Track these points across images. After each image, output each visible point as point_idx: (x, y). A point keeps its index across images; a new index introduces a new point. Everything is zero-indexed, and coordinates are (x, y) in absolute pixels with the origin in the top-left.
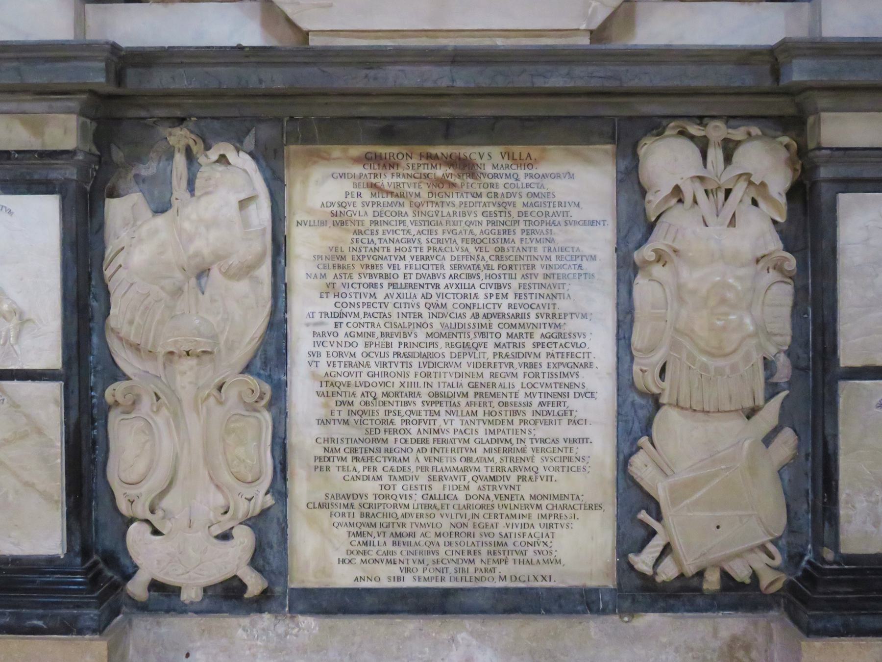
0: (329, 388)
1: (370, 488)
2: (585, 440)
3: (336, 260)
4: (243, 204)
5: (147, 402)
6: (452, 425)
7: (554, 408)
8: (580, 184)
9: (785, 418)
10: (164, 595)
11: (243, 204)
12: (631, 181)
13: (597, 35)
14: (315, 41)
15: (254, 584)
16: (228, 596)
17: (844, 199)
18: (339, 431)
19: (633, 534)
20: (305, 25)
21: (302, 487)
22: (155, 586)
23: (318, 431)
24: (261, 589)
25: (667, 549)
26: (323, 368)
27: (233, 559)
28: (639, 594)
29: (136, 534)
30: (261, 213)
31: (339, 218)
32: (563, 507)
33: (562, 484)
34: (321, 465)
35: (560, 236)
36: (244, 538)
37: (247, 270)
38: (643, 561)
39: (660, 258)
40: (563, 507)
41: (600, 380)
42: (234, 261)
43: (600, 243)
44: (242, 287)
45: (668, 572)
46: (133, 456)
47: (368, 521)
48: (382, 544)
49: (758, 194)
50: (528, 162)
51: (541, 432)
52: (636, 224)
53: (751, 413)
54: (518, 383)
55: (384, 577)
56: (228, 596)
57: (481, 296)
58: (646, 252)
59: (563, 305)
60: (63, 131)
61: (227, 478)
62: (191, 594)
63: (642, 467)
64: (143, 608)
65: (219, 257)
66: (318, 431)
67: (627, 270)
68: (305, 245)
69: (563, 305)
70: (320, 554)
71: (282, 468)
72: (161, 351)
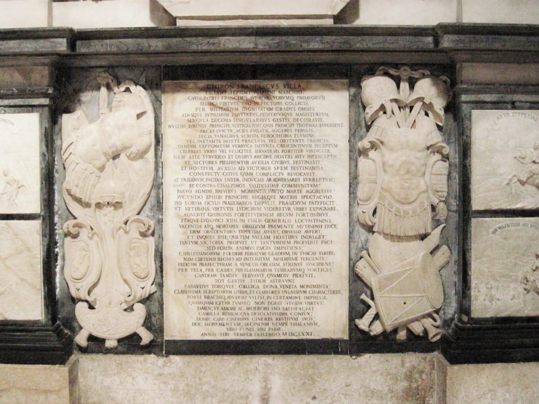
0: (187, 222)
1: (209, 281)
2: (331, 253)
3: (190, 147)
4: (139, 116)
5: (84, 234)
6: (255, 244)
7: (313, 234)
8: (329, 104)
9: (444, 240)
10: (96, 344)
11: (139, 116)
12: (358, 103)
13: (338, 18)
14: (180, 24)
15: (146, 337)
16: (130, 344)
17: (476, 113)
18: (191, 248)
19: (358, 308)
20: (174, 14)
21: (171, 282)
22: (91, 338)
23: (181, 248)
24: (150, 342)
25: (377, 317)
26: (183, 211)
27: (134, 323)
28: (360, 343)
29: (81, 309)
30: (149, 120)
31: (192, 124)
32: (320, 291)
33: (318, 279)
34: (183, 267)
35: (317, 132)
36: (140, 310)
37: (141, 155)
38: (363, 323)
39: (373, 146)
40: (320, 291)
41: (340, 218)
42: (134, 150)
43: (341, 136)
44: (138, 164)
45: (377, 329)
46: (77, 267)
47: (209, 301)
48: (216, 314)
49: (428, 109)
50: (299, 89)
51: (306, 248)
52: (361, 123)
53: (423, 237)
54: (293, 220)
55: (218, 334)
56: (130, 344)
57: (272, 168)
58: (365, 143)
59: (319, 174)
60: (41, 76)
61: (130, 277)
62: (110, 344)
63: (362, 269)
64: (84, 350)
65: (125, 148)
66: (181, 248)
67: (356, 154)
68: (172, 138)
69: (319, 174)
70: (182, 321)
71: (160, 269)
72: (93, 202)
